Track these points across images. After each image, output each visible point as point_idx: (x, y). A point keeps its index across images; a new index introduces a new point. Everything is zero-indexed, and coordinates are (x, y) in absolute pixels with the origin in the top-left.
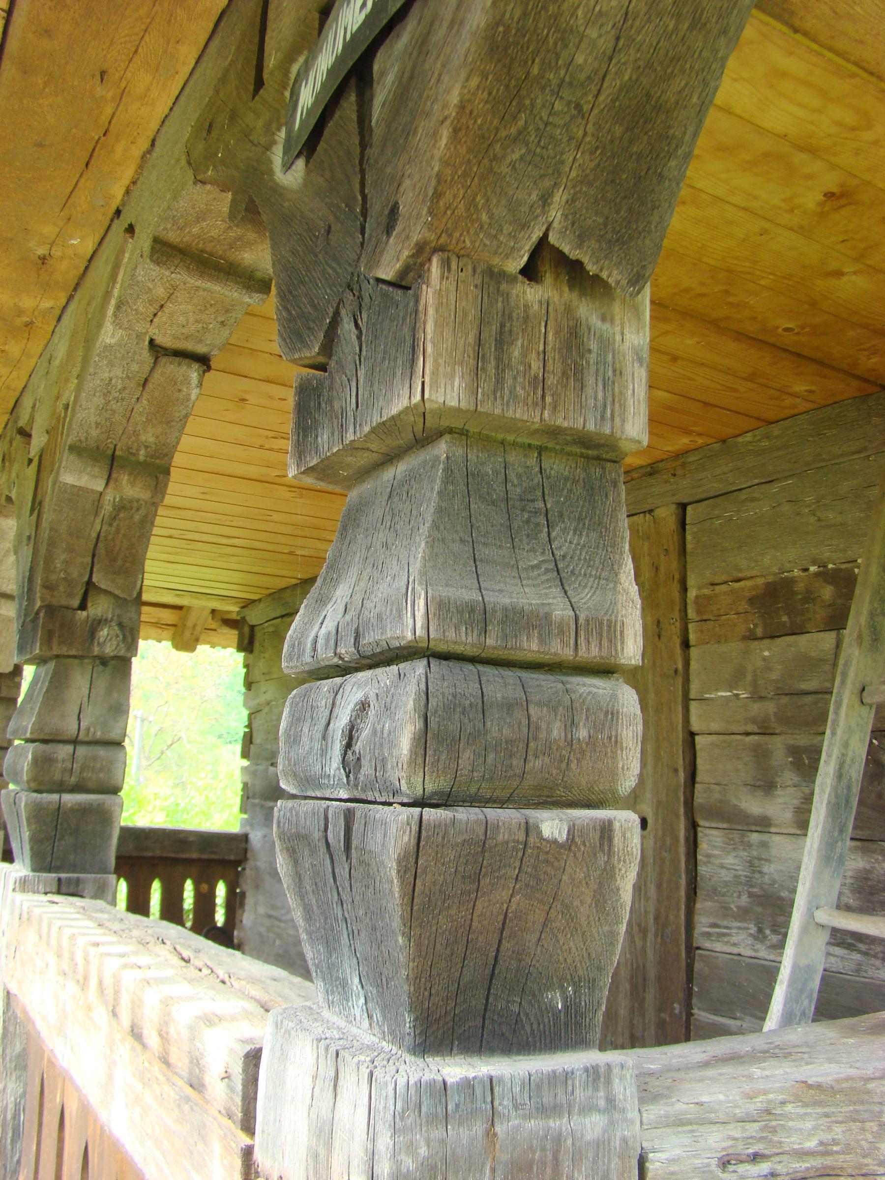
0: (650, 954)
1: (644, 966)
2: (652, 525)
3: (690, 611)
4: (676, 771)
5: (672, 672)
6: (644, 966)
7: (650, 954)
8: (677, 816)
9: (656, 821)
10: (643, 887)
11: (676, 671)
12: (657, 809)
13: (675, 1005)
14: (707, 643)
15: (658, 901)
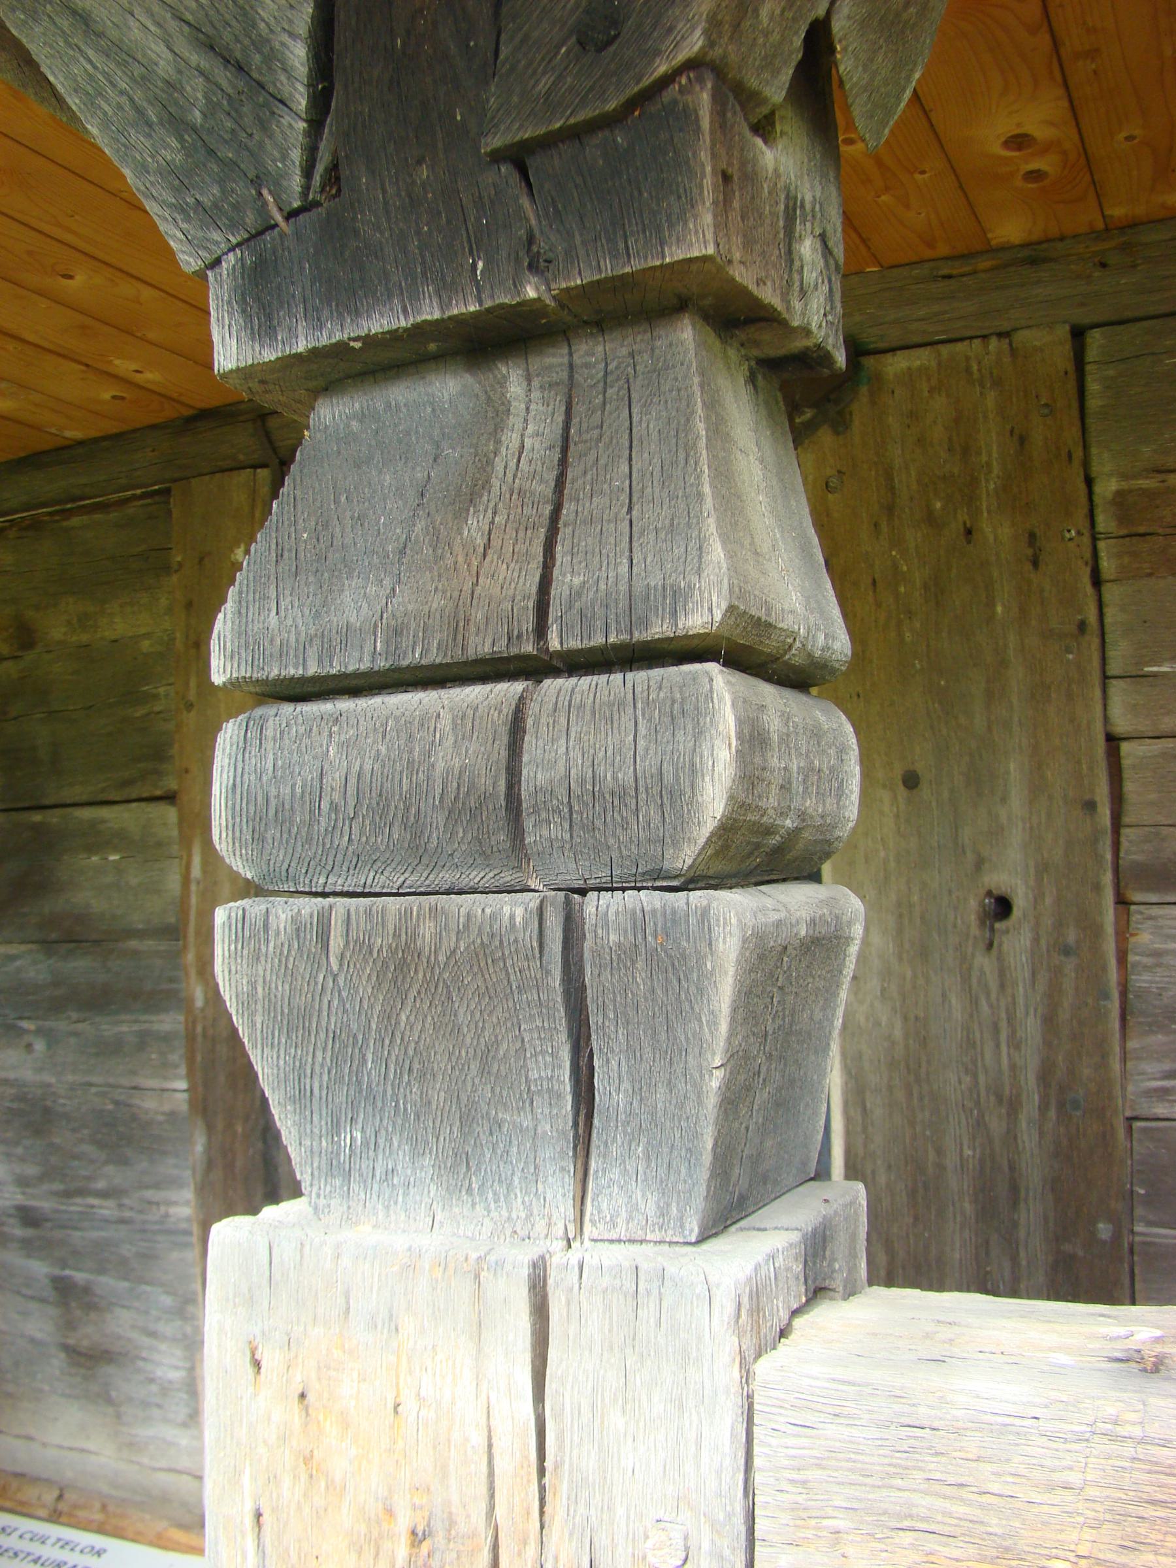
0: (1028, 1139)
1: (1012, 1168)
2: (1007, 360)
3: (1100, 518)
4: (1090, 806)
5: (1073, 628)
6: (1012, 1168)
7: (1028, 1139)
8: (1097, 888)
9: (1038, 898)
10: (1003, 1024)
11: (1082, 626)
12: (1039, 880)
13: (1101, 1226)
14: (1150, 575)
15: (1047, 1044)
